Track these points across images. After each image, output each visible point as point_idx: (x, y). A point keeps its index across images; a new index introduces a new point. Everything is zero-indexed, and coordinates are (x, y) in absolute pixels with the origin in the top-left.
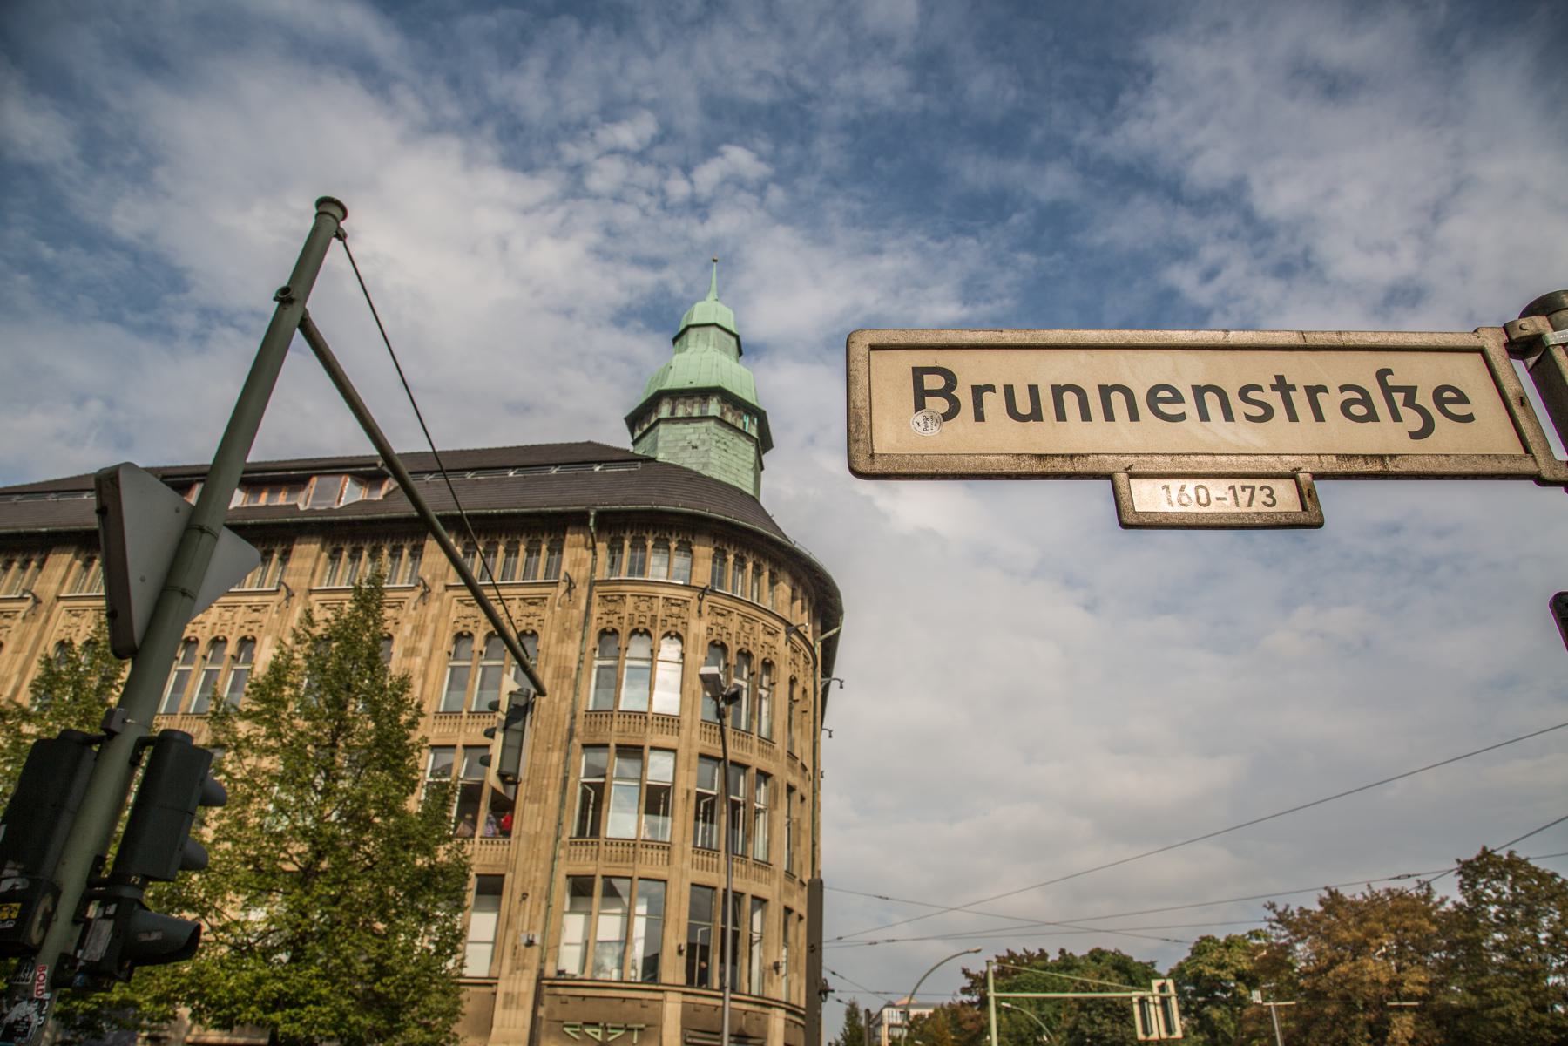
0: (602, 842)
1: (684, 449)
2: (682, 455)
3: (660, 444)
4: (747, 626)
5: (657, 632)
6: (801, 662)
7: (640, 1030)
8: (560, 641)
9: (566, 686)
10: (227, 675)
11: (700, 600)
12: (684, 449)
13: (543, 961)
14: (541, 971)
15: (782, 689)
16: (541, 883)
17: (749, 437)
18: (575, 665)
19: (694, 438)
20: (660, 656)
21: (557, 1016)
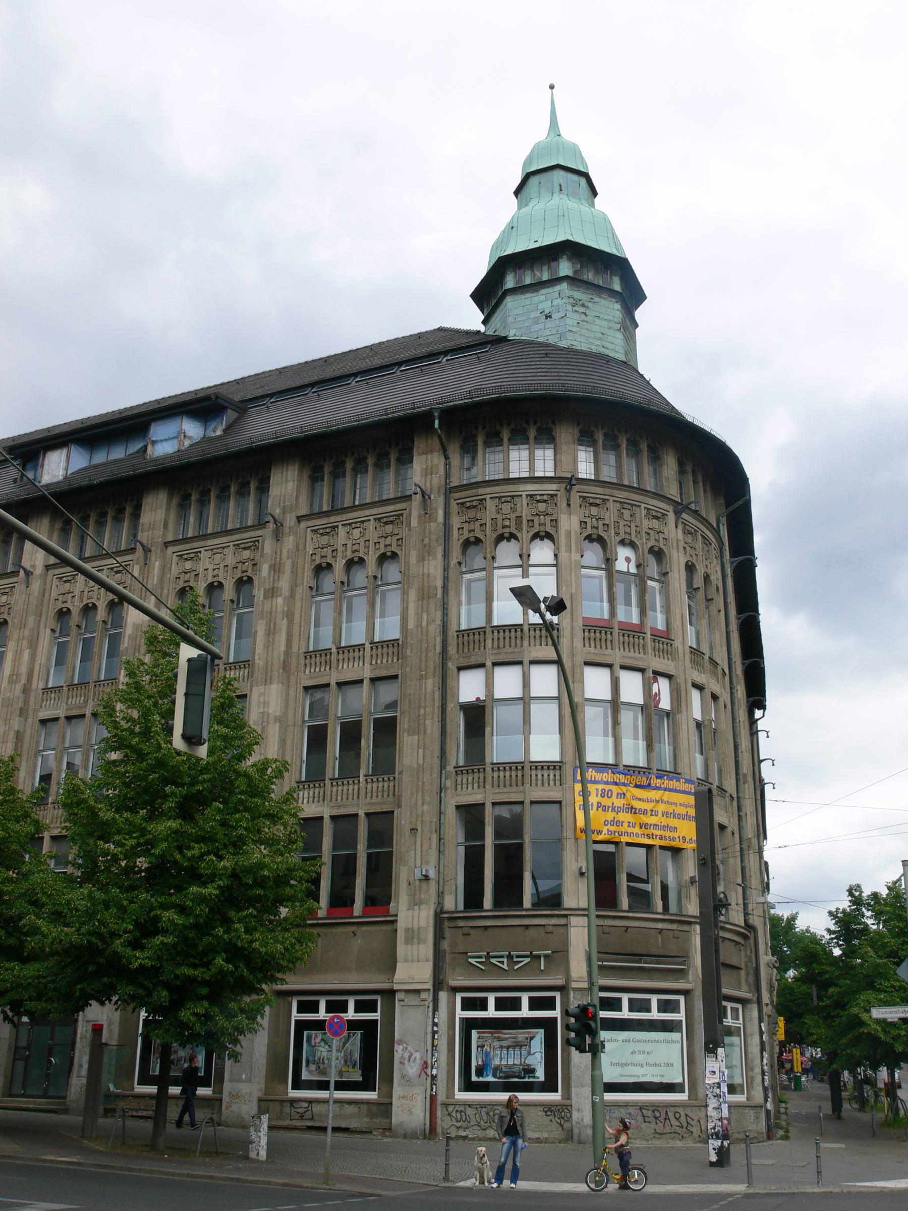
0: (488, 769)
1: (536, 321)
2: (535, 328)
3: (510, 320)
4: (627, 514)
5: (525, 535)
6: (699, 544)
7: (546, 956)
8: (421, 559)
9: (432, 608)
10: (102, 642)
11: (568, 491)
12: (536, 321)
13: (440, 895)
14: (440, 904)
15: (678, 578)
16: (430, 817)
17: (612, 293)
18: (439, 583)
19: (546, 306)
20: (532, 561)
21: (461, 949)
